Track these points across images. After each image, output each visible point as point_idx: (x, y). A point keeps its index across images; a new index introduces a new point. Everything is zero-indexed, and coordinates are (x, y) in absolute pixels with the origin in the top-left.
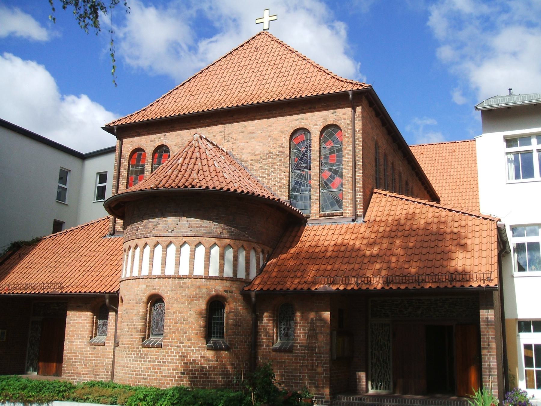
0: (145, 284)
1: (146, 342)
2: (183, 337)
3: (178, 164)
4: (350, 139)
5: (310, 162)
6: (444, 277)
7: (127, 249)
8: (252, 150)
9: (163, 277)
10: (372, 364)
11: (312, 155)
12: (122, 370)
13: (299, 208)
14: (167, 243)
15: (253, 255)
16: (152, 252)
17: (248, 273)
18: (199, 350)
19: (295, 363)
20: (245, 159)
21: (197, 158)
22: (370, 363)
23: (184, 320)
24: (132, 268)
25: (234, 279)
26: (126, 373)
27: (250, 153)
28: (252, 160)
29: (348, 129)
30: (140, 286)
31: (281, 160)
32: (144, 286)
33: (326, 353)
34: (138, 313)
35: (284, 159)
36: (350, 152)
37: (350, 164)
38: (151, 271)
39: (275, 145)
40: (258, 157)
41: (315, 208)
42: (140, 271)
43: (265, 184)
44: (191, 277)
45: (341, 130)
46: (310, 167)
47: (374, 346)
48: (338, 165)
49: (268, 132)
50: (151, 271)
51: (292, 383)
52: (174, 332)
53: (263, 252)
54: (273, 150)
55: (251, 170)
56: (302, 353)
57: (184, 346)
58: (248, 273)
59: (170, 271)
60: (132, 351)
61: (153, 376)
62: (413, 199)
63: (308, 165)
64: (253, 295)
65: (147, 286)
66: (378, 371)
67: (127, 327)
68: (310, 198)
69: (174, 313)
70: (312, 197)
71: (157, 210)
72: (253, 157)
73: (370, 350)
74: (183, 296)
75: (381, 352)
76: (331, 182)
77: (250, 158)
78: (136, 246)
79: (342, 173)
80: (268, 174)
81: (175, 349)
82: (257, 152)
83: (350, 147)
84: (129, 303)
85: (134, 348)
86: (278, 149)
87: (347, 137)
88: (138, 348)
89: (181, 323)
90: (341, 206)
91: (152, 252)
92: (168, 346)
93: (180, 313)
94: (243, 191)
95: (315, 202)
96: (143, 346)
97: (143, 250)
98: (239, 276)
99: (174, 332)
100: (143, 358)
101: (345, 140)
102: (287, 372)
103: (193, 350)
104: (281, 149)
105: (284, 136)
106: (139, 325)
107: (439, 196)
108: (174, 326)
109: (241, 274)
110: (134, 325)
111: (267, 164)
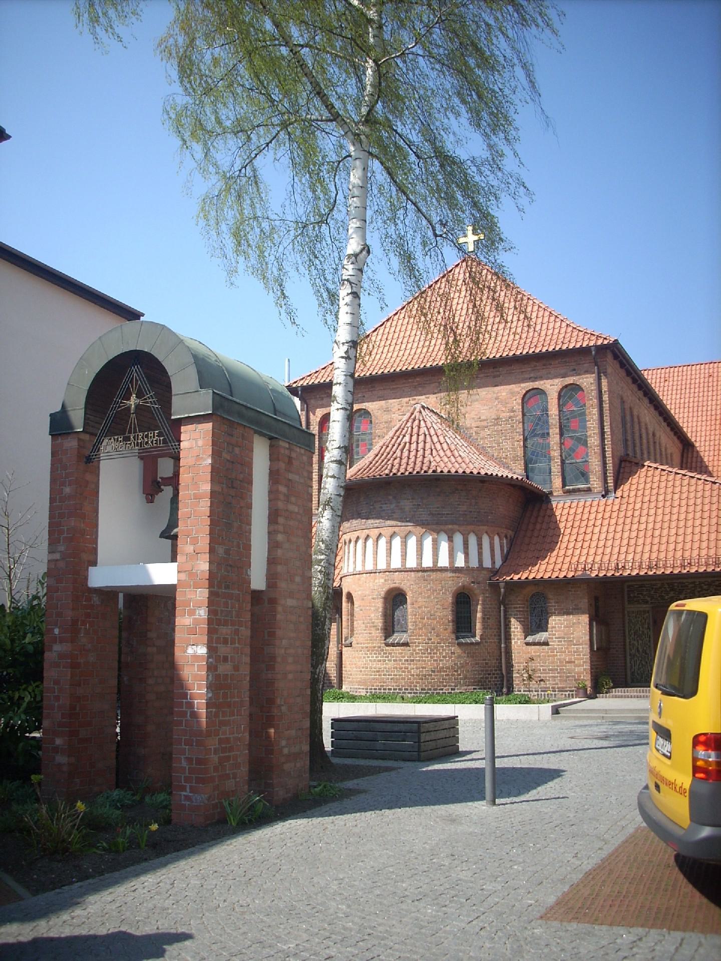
0: (382, 578)
1: (390, 640)
2: (431, 633)
3: (406, 443)
4: (595, 401)
5: (548, 429)
6: (711, 560)
7: (347, 541)
8: (476, 415)
9: (404, 570)
10: (630, 655)
11: (550, 421)
12: (361, 671)
13: (537, 483)
14: (405, 533)
15: (496, 539)
16: (389, 543)
17: (493, 563)
18: (449, 646)
19: (551, 656)
20: (469, 426)
21: (425, 435)
22: (628, 654)
23: (431, 615)
24: (355, 562)
25: (481, 567)
26: (366, 675)
27: (473, 418)
28: (478, 427)
29: (592, 390)
30: (377, 581)
31: (513, 426)
32: (383, 581)
33: (586, 644)
34: (377, 610)
35: (517, 426)
36: (596, 417)
37: (597, 431)
38: (389, 564)
39: (504, 409)
40: (484, 424)
41: (557, 482)
42: (364, 565)
43: (495, 455)
44: (435, 569)
45: (583, 391)
46: (548, 434)
47: (633, 636)
48: (583, 432)
49: (494, 393)
50: (389, 564)
51: (549, 677)
52: (420, 629)
53: (506, 537)
54: (503, 415)
55: (477, 439)
56: (558, 645)
57: (432, 643)
58: (493, 563)
59: (411, 563)
60: (373, 651)
61: (400, 675)
62: (670, 469)
63: (546, 431)
64: (502, 585)
65: (385, 580)
66: (638, 662)
67: (364, 626)
68: (550, 473)
69: (419, 607)
70: (553, 469)
71: (391, 497)
72: (479, 424)
73: (628, 641)
74: (428, 590)
75: (640, 642)
76: (574, 451)
77: (474, 425)
78: (368, 537)
79: (587, 441)
80: (498, 444)
81: (422, 646)
82: (483, 418)
83: (595, 411)
84: (363, 599)
85: (374, 647)
86: (508, 414)
87: (591, 399)
88: (380, 647)
89: (428, 619)
90: (587, 481)
91: (389, 543)
92: (415, 643)
93: (425, 607)
94: (486, 474)
95: (556, 475)
96: (387, 645)
97: (377, 541)
98: (471, 565)
99: (420, 629)
100: (388, 657)
101: (588, 403)
102: (542, 666)
103: (443, 647)
104: (512, 414)
105: (514, 398)
106: (379, 623)
107: (693, 440)
108: (420, 622)
109: (487, 564)
110: (373, 623)
111: (495, 431)
